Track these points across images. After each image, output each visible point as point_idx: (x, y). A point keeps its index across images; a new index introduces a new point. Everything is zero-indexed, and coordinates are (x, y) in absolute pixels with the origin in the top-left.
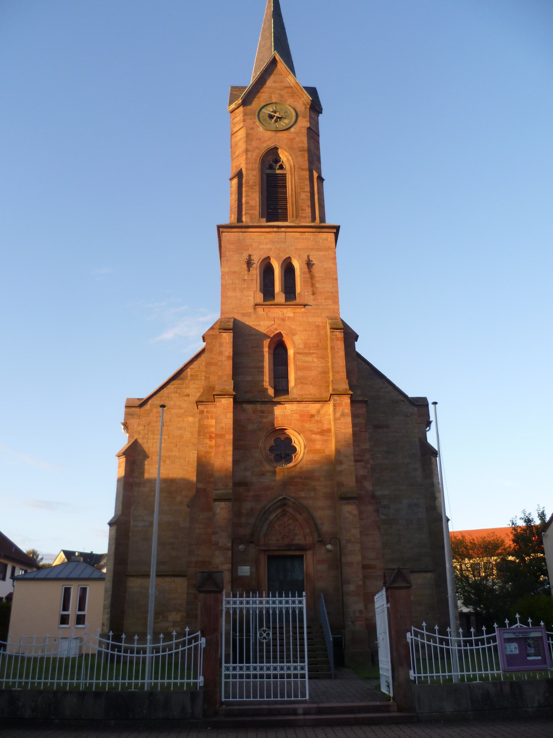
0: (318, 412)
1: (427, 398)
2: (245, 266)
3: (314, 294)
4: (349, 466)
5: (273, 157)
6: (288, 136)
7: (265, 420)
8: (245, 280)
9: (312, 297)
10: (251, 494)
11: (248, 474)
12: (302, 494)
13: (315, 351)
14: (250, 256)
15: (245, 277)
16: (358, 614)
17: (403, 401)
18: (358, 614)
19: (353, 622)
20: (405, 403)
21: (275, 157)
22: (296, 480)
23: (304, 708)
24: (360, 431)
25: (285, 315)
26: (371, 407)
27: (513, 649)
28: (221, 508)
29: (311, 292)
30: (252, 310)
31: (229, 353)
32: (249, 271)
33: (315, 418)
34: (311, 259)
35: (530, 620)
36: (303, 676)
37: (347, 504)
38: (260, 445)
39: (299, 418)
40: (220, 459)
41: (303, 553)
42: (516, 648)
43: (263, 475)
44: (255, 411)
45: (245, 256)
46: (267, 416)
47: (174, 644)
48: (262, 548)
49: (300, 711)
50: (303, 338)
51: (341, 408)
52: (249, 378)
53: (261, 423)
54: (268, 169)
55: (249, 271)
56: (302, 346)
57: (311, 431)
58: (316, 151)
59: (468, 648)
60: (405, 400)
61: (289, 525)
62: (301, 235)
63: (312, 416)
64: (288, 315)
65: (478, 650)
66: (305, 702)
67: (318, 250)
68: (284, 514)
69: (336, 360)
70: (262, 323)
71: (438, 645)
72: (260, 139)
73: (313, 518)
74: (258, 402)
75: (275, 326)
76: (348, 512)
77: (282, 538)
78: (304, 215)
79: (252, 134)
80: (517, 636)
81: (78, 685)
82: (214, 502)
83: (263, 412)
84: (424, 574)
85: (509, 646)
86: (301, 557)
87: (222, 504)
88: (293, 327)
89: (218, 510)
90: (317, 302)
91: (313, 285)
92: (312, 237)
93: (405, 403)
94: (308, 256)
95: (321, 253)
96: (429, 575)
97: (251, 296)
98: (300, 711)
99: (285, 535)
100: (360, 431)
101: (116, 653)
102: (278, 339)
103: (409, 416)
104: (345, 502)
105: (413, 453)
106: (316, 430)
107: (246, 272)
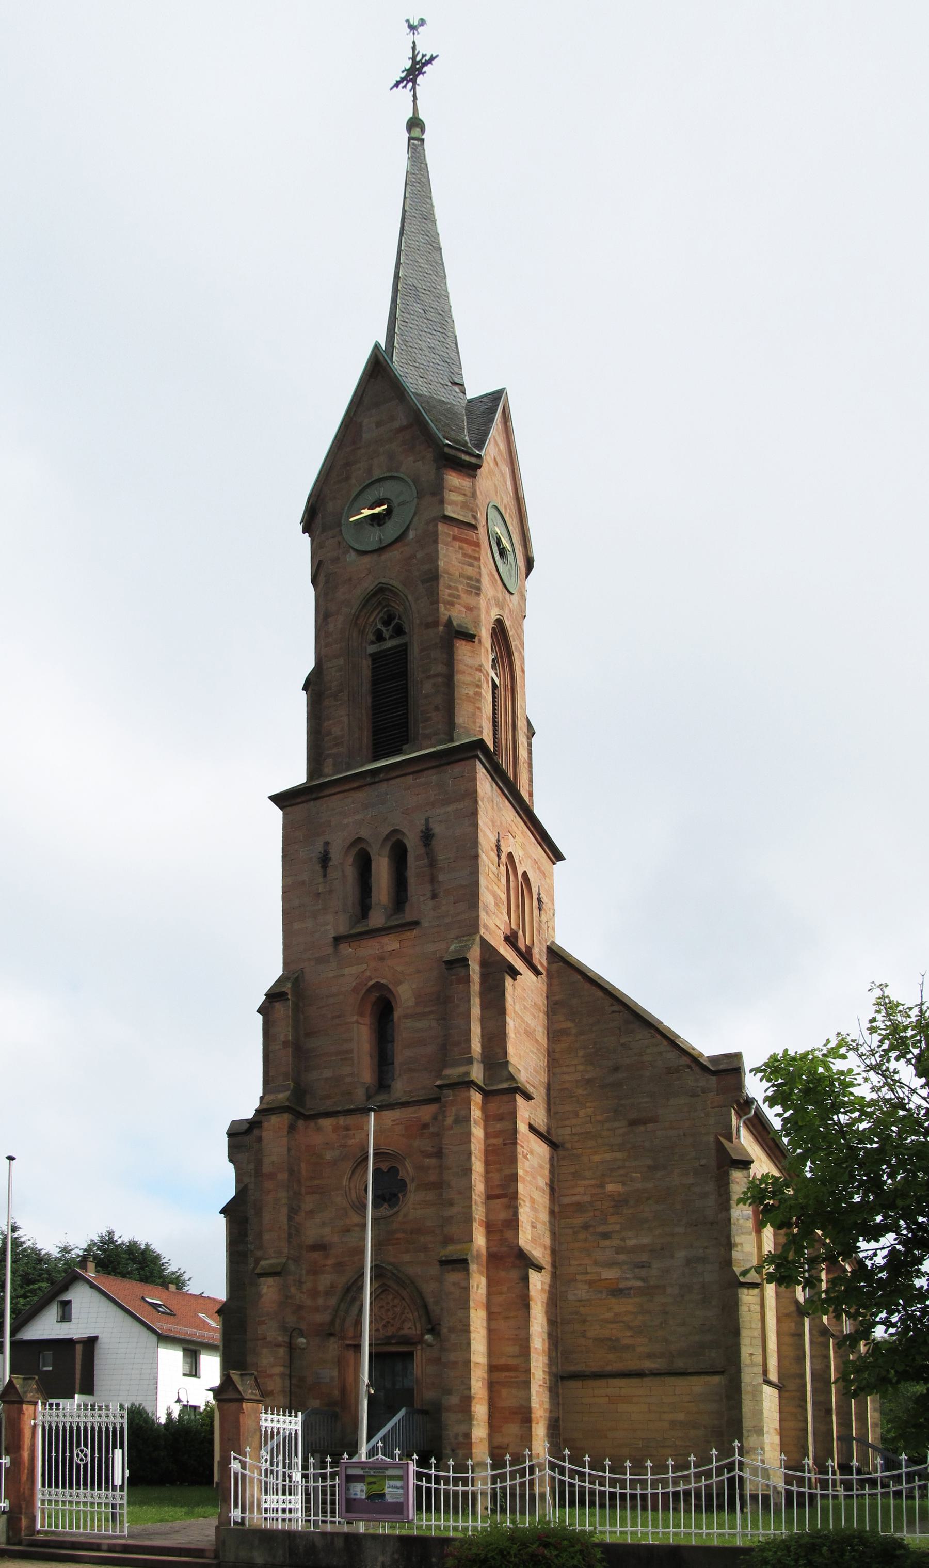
0: (435, 1118)
1: (744, 1055)
2: (318, 868)
3: (434, 896)
4: (463, 1207)
5: (381, 610)
6: (402, 552)
7: (351, 1142)
8: (319, 893)
9: (431, 903)
10: (330, 1262)
11: (327, 1231)
12: (407, 1258)
13: (433, 1008)
14: (327, 844)
15: (320, 889)
16: (461, 1439)
17: (689, 1067)
18: (461, 1439)
19: (453, 1450)
20: (692, 1070)
21: (385, 609)
22: (400, 1235)
23: (109, 1545)
24: (505, 1144)
25: (385, 949)
26: (625, 1087)
27: (358, 1493)
28: (269, 1287)
29: (429, 895)
30: (330, 950)
31: (286, 1035)
32: (325, 876)
33: (429, 1129)
34: (432, 825)
35: (397, 1452)
36: (121, 1506)
37: (453, 1270)
38: (344, 1184)
39: (403, 1132)
40: (270, 1212)
41: (413, 1349)
42: (362, 1491)
43: (348, 1231)
44: (336, 1129)
45: (319, 847)
46: (354, 1134)
47: (726, 1480)
48: (348, 1342)
49: (105, 1547)
50: (414, 986)
51: (454, 1109)
52: (327, 1073)
53: (344, 1146)
54: (372, 643)
55: (325, 876)
56: (411, 1003)
57: (422, 1152)
58: (466, 567)
59: (442, 1487)
60: (693, 1065)
61: (395, 1306)
62: (416, 779)
63: (425, 1126)
64: (390, 948)
65: (456, 1494)
66: (124, 1537)
67: (446, 802)
68: (386, 1290)
69: (455, 1022)
70: (346, 971)
71: (433, 1485)
72: (350, 580)
73: (420, 1294)
74: (338, 1112)
75: (368, 974)
76: (454, 1284)
77: (384, 1326)
78: (428, 731)
79: (336, 572)
80: (366, 1472)
81: (465, 1529)
82: (259, 1278)
83: (347, 1128)
84: (708, 1378)
85: (354, 1487)
86: (410, 1355)
87: (270, 1280)
88: (399, 968)
89: (265, 1290)
90: (440, 911)
91: (433, 880)
92: (434, 778)
93: (692, 1070)
94: (427, 820)
95: (450, 809)
96: (716, 1379)
97: (328, 924)
98: (105, 1547)
99: (388, 1322)
100: (505, 1144)
101: (618, 1490)
102: (377, 995)
103: (699, 1096)
104: (450, 1267)
105: (702, 1166)
106: (431, 1149)
107: (321, 880)
